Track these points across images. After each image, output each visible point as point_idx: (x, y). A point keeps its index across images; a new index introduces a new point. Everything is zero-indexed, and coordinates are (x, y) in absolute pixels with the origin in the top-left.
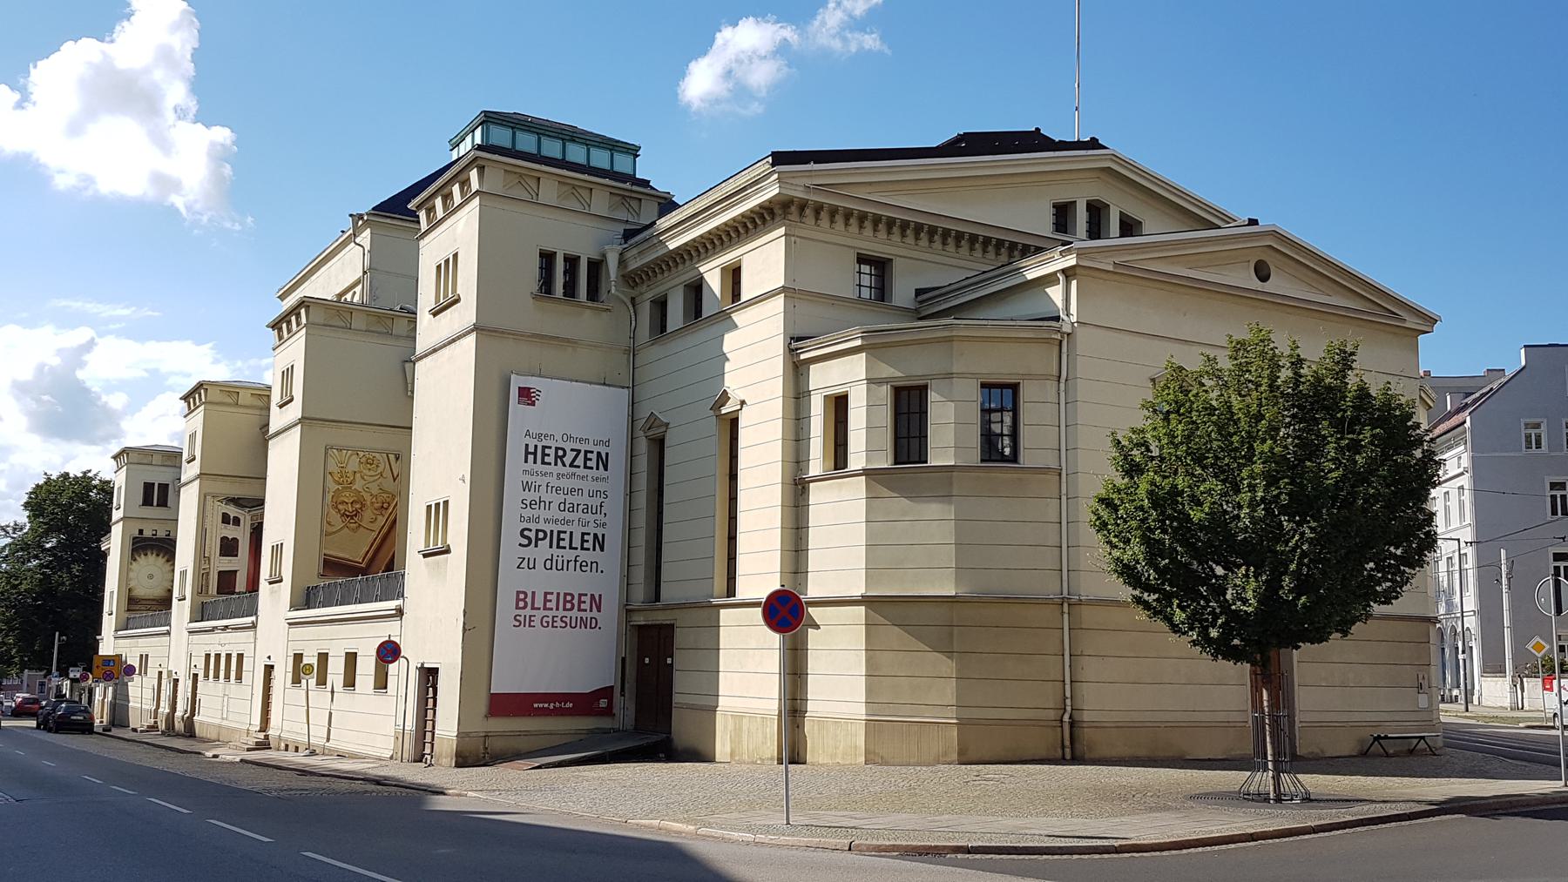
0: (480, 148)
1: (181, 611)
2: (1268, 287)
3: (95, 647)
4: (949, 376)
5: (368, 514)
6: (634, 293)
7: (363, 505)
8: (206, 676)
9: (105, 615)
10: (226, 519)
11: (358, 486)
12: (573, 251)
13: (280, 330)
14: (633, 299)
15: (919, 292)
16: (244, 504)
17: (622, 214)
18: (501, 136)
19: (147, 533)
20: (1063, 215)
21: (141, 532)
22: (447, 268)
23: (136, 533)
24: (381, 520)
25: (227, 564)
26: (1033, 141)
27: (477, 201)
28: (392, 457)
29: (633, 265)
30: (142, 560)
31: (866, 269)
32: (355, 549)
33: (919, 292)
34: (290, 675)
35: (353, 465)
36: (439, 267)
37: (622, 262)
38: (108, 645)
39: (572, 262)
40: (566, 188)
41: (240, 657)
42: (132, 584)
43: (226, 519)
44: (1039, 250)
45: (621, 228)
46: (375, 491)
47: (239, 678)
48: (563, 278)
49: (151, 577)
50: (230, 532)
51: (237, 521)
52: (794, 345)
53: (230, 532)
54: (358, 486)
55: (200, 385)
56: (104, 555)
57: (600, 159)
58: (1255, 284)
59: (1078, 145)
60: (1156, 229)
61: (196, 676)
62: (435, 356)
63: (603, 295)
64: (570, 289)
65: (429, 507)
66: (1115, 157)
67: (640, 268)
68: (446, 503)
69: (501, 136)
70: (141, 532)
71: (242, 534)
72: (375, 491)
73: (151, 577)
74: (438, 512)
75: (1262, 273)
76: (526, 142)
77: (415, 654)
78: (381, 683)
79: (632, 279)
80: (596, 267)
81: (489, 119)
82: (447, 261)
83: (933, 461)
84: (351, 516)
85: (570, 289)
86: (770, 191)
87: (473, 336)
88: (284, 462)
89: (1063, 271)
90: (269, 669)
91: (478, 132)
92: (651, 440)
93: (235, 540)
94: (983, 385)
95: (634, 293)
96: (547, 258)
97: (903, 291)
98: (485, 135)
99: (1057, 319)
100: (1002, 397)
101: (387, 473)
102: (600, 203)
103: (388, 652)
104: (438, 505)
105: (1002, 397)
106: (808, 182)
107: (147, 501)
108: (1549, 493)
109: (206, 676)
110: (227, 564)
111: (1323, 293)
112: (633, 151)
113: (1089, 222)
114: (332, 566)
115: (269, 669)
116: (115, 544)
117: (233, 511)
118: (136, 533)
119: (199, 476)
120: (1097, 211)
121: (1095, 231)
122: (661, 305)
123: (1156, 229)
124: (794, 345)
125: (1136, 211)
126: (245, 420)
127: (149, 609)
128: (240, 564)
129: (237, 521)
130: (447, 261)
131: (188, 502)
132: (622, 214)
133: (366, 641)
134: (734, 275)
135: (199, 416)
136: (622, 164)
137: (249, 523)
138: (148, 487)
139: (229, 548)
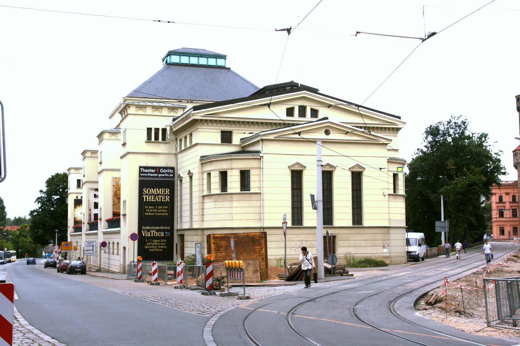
4: (232, 169)
13: (122, 114)
15: (241, 139)
21: (77, 197)
23: (75, 198)
29: (174, 130)
33: (241, 139)
39: (157, 130)
42: (76, 216)
45: (172, 118)
57: (212, 62)
61: (221, 294)
64: (157, 138)
70: (77, 197)
75: (327, 132)
80: (164, 130)
83: (252, 190)
85: (157, 138)
89: (261, 140)
96: (149, 130)
97: (236, 139)
100: (245, 176)
105: (245, 176)
106: (202, 114)
112: (224, 57)
136: (220, 62)
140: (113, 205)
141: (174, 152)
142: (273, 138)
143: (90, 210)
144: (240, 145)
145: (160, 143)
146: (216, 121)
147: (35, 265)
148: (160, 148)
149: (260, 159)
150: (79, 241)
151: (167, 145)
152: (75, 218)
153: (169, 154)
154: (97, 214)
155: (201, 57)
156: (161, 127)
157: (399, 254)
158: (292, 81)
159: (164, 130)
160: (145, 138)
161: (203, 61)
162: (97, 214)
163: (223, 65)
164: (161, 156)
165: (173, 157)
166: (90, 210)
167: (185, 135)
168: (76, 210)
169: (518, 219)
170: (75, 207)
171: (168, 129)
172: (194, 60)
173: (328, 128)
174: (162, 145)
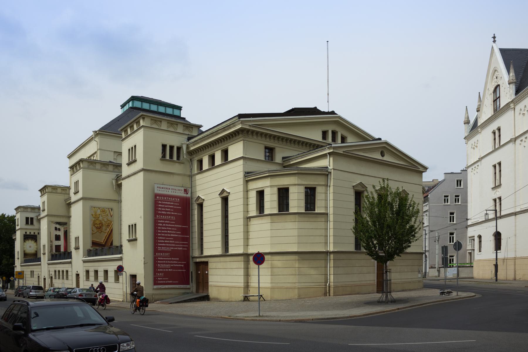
0: (131, 108)
1: (45, 259)
2: (385, 158)
3: (13, 269)
5: (104, 228)
6: (191, 157)
7: (102, 225)
8: (55, 278)
9: (16, 259)
10: (56, 229)
11: (101, 218)
12: (172, 144)
14: (191, 159)
15: (283, 158)
16: (62, 225)
17: (187, 132)
18: (138, 104)
19: (28, 233)
20: (325, 134)
21: (26, 233)
22: (133, 150)
23: (25, 233)
24: (108, 230)
25: (57, 243)
26: (314, 111)
27: (142, 129)
29: (192, 148)
31: (267, 150)
32: (101, 239)
33: (283, 158)
34: (85, 277)
35: (99, 212)
36: (129, 150)
37: (188, 147)
38: (18, 268)
39: (172, 148)
40: (153, 121)
41: (67, 271)
42: (25, 249)
43: (56, 229)
44: (322, 146)
45: (186, 137)
46: (106, 220)
47: (67, 278)
48: (169, 153)
49: (30, 247)
50: (58, 233)
51: (59, 230)
52: (246, 175)
53: (58, 233)
54: (101, 218)
56: (13, 241)
57: (169, 111)
58: (381, 158)
59: (328, 113)
60: (351, 140)
61: (52, 277)
63: (181, 158)
64: (171, 156)
65: (129, 226)
66: (340, 117)
67: (194, 150)
68: (135, 225)
69: (138, 104)
70: (26, 233)
71: (61, 234)
72: (106, 220)
73: (30, 247)
74: (133, 228)
75: (383, 155)
76: (146, 106)
77: (129, 270)
78: (117, 279)
79: (191, 153)
80: (179, 149)
81: (133, 99)
82: (132, 148)
83: (291, 210)
85: (171, 156)
86: (239, 126)
87: (142, 173)
88: (77, 213)
89: (329, 153)
90: (78, 275)
91: (131, 103)
92: (198, 204)
93: (59, 236)
94: (306, 188)
95: (191, 157)
96: (164, 146)
97: (278, 158)
98: (133, 104)
99: (327, 167)
101: (109, 215)
102: (180, 129)
103: (120, 269)
104: (132, 225)
106: (250, 124)
107: (27, 223)
108: (449, 216)
109: (55, 278)
110: (57, 243)
111: (398, 160)
112: (180, 108)
113: (332, 137)
114: (94, 244)
115: (78, 275)
116: (18, 236)
117: (58, 226)
119: (47, 216)
120: (334, 133)
121: (334, 140)
122: (201, 162)
123: (351, 140)
124: (246, 175)
125: (346, 134)
126: (60, 198)
127: (32, 258)
128: (61, 243)
129: (59, 230)
130: (132, 148)
131: (44, 225)
132: (187, 132)
133: (112, 267)
134: (225, 153)
135: (45, 198)
136: (176, 112)
137: (63, 230)
138: (27, 219)
139: (58, 238)
140: (92, 234)
141: (189, 173)
142: (342, 152)
143: (51, 242)
144: (283, 164)
145: (174, 162)
146: (262, 134)
147: (6, 302)
148: (176, 168)
149: (328, 175)
150: (70, 270)
151: (182, 165)
152: (24, 251)
153: (184, 175)
154: (60, 246)
155: (161, 105)
156: (176, 144)
157: (368, 282)
158: (316, 107)
159: (179, 149)
160: (160, 155)
161: (162, 109)
162: (60, 246)
163: (179, 115)
164: (176, 177)
165: (187, 179)
166: (51, 242)
167: (211, 152)
168: (25, 244)
169: (468, 251)
170: (24, 241)
171: (184, 147)
172: (154, 108)
173: (383, 150)
174: (177, 165)
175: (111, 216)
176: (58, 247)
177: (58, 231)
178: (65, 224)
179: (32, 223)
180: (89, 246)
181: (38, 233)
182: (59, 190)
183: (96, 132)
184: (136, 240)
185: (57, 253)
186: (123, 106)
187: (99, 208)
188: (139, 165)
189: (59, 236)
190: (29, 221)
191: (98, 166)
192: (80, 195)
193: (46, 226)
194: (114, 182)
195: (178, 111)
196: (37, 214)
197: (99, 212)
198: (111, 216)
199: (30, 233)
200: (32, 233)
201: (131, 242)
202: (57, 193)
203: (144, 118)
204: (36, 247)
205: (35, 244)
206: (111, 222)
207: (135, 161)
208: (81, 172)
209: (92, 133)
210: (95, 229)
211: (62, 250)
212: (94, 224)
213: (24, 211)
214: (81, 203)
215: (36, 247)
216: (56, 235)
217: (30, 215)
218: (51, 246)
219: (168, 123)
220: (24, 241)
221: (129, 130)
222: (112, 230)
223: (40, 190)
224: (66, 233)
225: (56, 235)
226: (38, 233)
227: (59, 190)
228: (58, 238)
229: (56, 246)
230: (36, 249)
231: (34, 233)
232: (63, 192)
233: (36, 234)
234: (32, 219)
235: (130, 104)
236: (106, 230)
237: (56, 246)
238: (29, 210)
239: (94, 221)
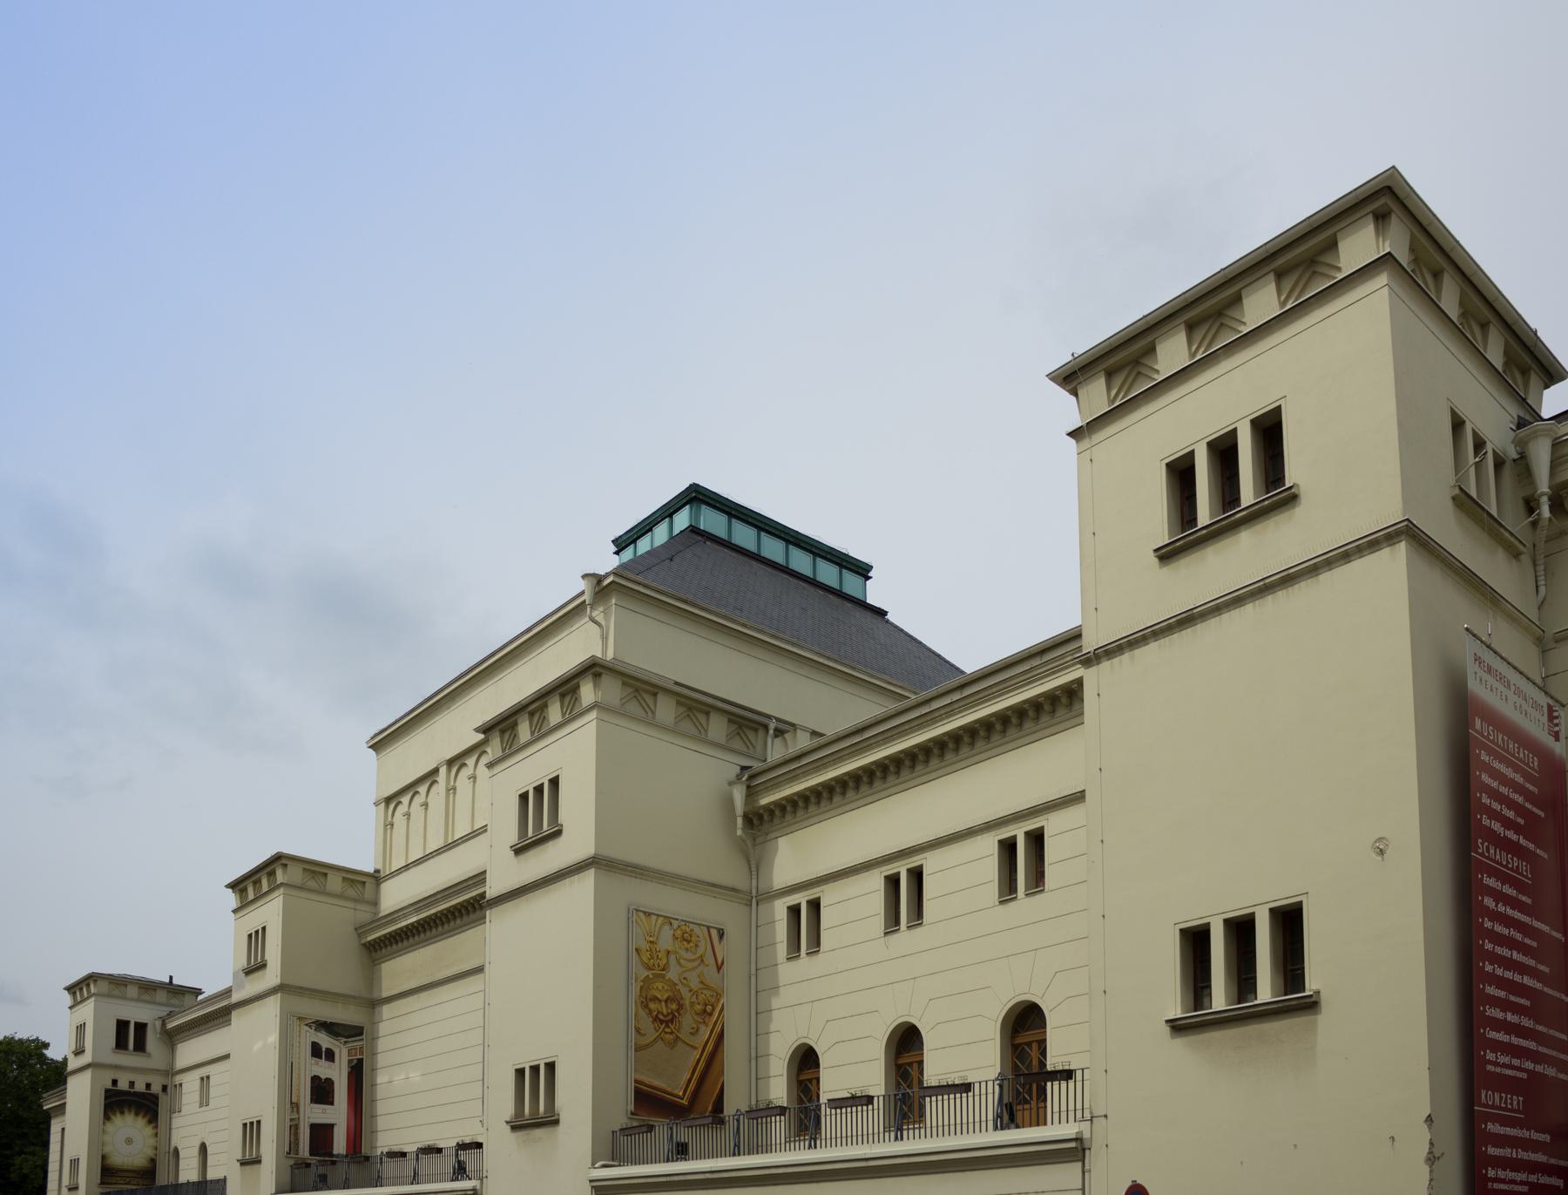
5: (687, 1021)
7: (680, 1006)
10: (316, 1051)
18: (713, 522)
19: (123, 1085)
21: (115, 1082)
23: (109, 1085)
24: (705, 1033)
27: (281, 890)
28: (714, 933)
30: (118, 1120)
32: (676, 1082)
35: (666, 940)
36: (524, 797)
42: (107, 1149)
43: (316, 1051)
50: (323, 1069)
51: (330, 1056)
53: (323, 1069)
54: (673, 974)
55: (278, 858)
57: (828, 573)
62: (1187, 634)
68: (551, 1067)
69: (713, 522)
70: (115, 1082)
71: (338, 1073)
72: (695, 984)
73: (129, 1141)
74: (75, 1163)
84: (666, 1021)
87: (588, 879)
98: (695, 516)
107: (121, 1044)
110: (317, 1114)
112: (863, 571)
114: (648, 1101)
117: (325, 1041)
118: (109, 1085)
128: (337, 1114)
129: (330, 1056)
136: (851, 584)
137: (345, 1059)
138: (122, 1026)
139: (322, 1091)
143: (295, 1106)
152: (104, 1157)
154: (330, 1127)
155: (798, 545)
162: (330, 1127)
170: (107, 1117)
175: (719, 968)
176: (322, 1134)
177: (323, 1062)
178: (355, 1032)
179: (140, 1046)
180: (621, 1110)
181: (165, 1088)
182: (334, 883)
183: (598, 579)
184: (257, 1161)
185: (314, 1160)
186: (621, 544)
187: (669, 920)
188: (271, 976)
189: (330, 1082)
190: (128, 1036)
191: (666, 710)
192: (87, 1058)
193: (273, 1038)
194: (739, 795)
195: (858, 580)
196: (163, 1011)
197: (666, 940)
198: (719, 968)
199: (132, 1084)
200: (140, 1087)
201: (248, 1168)
202: (323, 892)
203: (597, 676)
204: (152, 1141)
205: (149, 1130)
206: (718, 996)
207: (262, 966)
208: (593, 726)
209: (582, 585)
210: (647, 1024)
211: (340, 1145)
212: (646, 1000)
213: (109, 996)
214: (88, 1075)
215: (152, 1141)
216: (315, 1079)
217: (137, 1012)
218: (294, 1128)
219: (678, 703)
220: (107, 1117)
221: (265, 882)
222: (721, 1035)
223: (233, 886)
224: (357, 1073)
225: (315, 1079)
226: (165, 1088)
227: (334, 883)
228: (322, 1091)
229: (314, 1127)
230: (150, 1153)
231: (148, 1086)
232: (351, 892)
233: (156, 1089)
234: (141, 1028)
235: (682, 520)
236: (695, 1032)
237: (314, 1127)
238: (132, 991)
239: (646, 984)
